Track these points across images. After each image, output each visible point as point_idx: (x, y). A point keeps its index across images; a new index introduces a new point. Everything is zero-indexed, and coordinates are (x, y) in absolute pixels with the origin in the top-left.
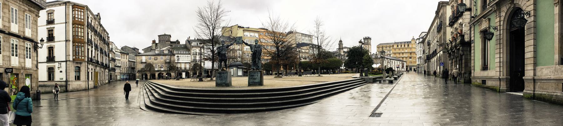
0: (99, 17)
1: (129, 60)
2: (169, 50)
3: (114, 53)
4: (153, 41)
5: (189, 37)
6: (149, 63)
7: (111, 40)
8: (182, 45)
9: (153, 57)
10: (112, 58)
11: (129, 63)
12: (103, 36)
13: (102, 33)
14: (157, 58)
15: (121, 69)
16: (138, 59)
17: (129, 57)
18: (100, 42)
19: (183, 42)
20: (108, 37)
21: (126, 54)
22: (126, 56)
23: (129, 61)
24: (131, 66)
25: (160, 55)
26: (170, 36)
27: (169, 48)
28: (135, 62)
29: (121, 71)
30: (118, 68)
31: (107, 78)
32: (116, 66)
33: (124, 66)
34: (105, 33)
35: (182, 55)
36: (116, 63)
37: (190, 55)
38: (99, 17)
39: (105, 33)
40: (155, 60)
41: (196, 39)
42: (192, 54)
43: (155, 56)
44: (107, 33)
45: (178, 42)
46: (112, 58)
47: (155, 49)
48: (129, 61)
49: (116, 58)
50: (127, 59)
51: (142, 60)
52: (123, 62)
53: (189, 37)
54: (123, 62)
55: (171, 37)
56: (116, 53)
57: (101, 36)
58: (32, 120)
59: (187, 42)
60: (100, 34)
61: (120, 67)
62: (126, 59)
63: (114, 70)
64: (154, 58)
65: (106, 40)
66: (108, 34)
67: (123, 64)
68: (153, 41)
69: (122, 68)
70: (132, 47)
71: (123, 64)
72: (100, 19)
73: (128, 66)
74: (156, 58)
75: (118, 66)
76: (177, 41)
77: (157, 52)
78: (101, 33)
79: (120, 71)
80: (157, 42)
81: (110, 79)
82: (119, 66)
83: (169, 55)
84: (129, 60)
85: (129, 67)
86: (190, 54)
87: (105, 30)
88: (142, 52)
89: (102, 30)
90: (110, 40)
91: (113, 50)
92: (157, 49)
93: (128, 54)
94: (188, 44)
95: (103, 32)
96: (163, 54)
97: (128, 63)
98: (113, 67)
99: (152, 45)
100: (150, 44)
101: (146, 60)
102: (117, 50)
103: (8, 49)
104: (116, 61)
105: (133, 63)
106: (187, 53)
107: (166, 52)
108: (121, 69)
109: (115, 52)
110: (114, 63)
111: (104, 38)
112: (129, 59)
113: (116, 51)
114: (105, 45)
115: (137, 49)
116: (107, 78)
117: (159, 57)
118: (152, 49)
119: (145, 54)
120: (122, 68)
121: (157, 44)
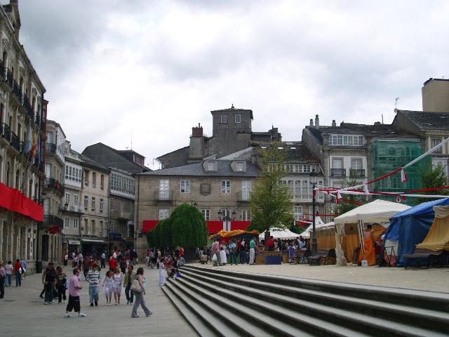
0: (13, 14)
1: (109, 191)
2: (249, 162)
3: (61, 165)
4: (193, 129)
5: (317, 116)
6: (182, 206)
7: (51, 115)
8: (292, 146)
9: (197, 185)
10: (52, 180)
11: (111, 206)
12: (23, 91)
13: (21, 79)
14: (210, 189)
15: (83, 222)
16: (146, 188)
17: (110, 183)
18: (12, 114)
19: (292, 134)
20: (44, 103)
21: (99, 169)
22: (102, 176)
23: (111, 195)
24: (117, 212)
25: (220, 177)
26: (248, 114)
27: (249, 156)
28: (133, 201)
29: (81, 229)
30: (71, 222)
31: (31, 254)
32: (64, 212)
33: (93, 213)
34: (33, 86)
35: (295, 179)
36: (65, 199)
37: (322, 179)
38: (13, 14)
39: (33, 86)
40: (202, 193)
41: (338, 125)
42: (329, 174)
43: (205, 181)
44: (39, 84)
45: (274, 134)
46: (52, 180)
47: (200, 156)
48: (111, 195)
49: (68, 182)
50: (106, 187)
51: (157, 192)
52: (90, 200)
53: (317, 116)
54: (90, 200)
55: (252, 118)
56: (67, 164)
57: (17, 91)
58: (129, 149)
59: (308, 132)
60: (16, 84)
61: (79, 214)
62: (102, 189)
63: (56, 225)
64: (201, 188)
65: (36, 110)
66: (43, 91)
67: (90, 205)
68: (193, 129)
69: (86, 220)
70: (120, 146)
71: (90, 205)
72: (17, 24)
73: (105, 214)
74: (206, 188)
75: (72, 214)
76: (274, 131)
77: (211, 167)
78: (17, 77)
79: (77, 229)
80: (208, 132)
81: (40, 256)
82: (76, 210)
83: (248, 178)
84: (112, 191)
85: (109, 218)
86: (321, 174)
87: (32, 74)
88: (154, 166)
89: (23, 71)
90: (49, 117)
91: (58, 153)
92: (208, 156)
93: (108, 172)
94: (312, 140)
95: (26, 79)
96: (230, 174)
97: (106, 200)
98: (55, 212)
99: (191, 142)
100: (182, 140)
101: (172, 192)
102: (70, 156)
103: (141, 187)
104: (66, 192)
105: (122, 205)
106: (294, 171)
107: (240, 168)
108: (83, 222)
109: (63, 160)
110: (57, 199)
111: (27, 100)
112: (110, 187)
113: (67, 159)
114: (18, 114)
115: (137, 155)
116: (31, 254)
117: (216, 185)
118: (191, 156)
119: (170, 171)
120: (86, 220)
121: (206, 139)
